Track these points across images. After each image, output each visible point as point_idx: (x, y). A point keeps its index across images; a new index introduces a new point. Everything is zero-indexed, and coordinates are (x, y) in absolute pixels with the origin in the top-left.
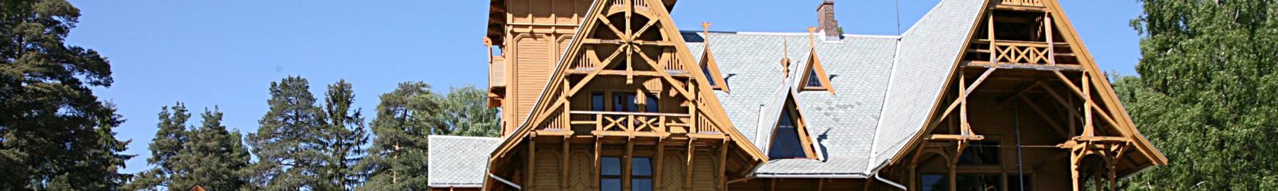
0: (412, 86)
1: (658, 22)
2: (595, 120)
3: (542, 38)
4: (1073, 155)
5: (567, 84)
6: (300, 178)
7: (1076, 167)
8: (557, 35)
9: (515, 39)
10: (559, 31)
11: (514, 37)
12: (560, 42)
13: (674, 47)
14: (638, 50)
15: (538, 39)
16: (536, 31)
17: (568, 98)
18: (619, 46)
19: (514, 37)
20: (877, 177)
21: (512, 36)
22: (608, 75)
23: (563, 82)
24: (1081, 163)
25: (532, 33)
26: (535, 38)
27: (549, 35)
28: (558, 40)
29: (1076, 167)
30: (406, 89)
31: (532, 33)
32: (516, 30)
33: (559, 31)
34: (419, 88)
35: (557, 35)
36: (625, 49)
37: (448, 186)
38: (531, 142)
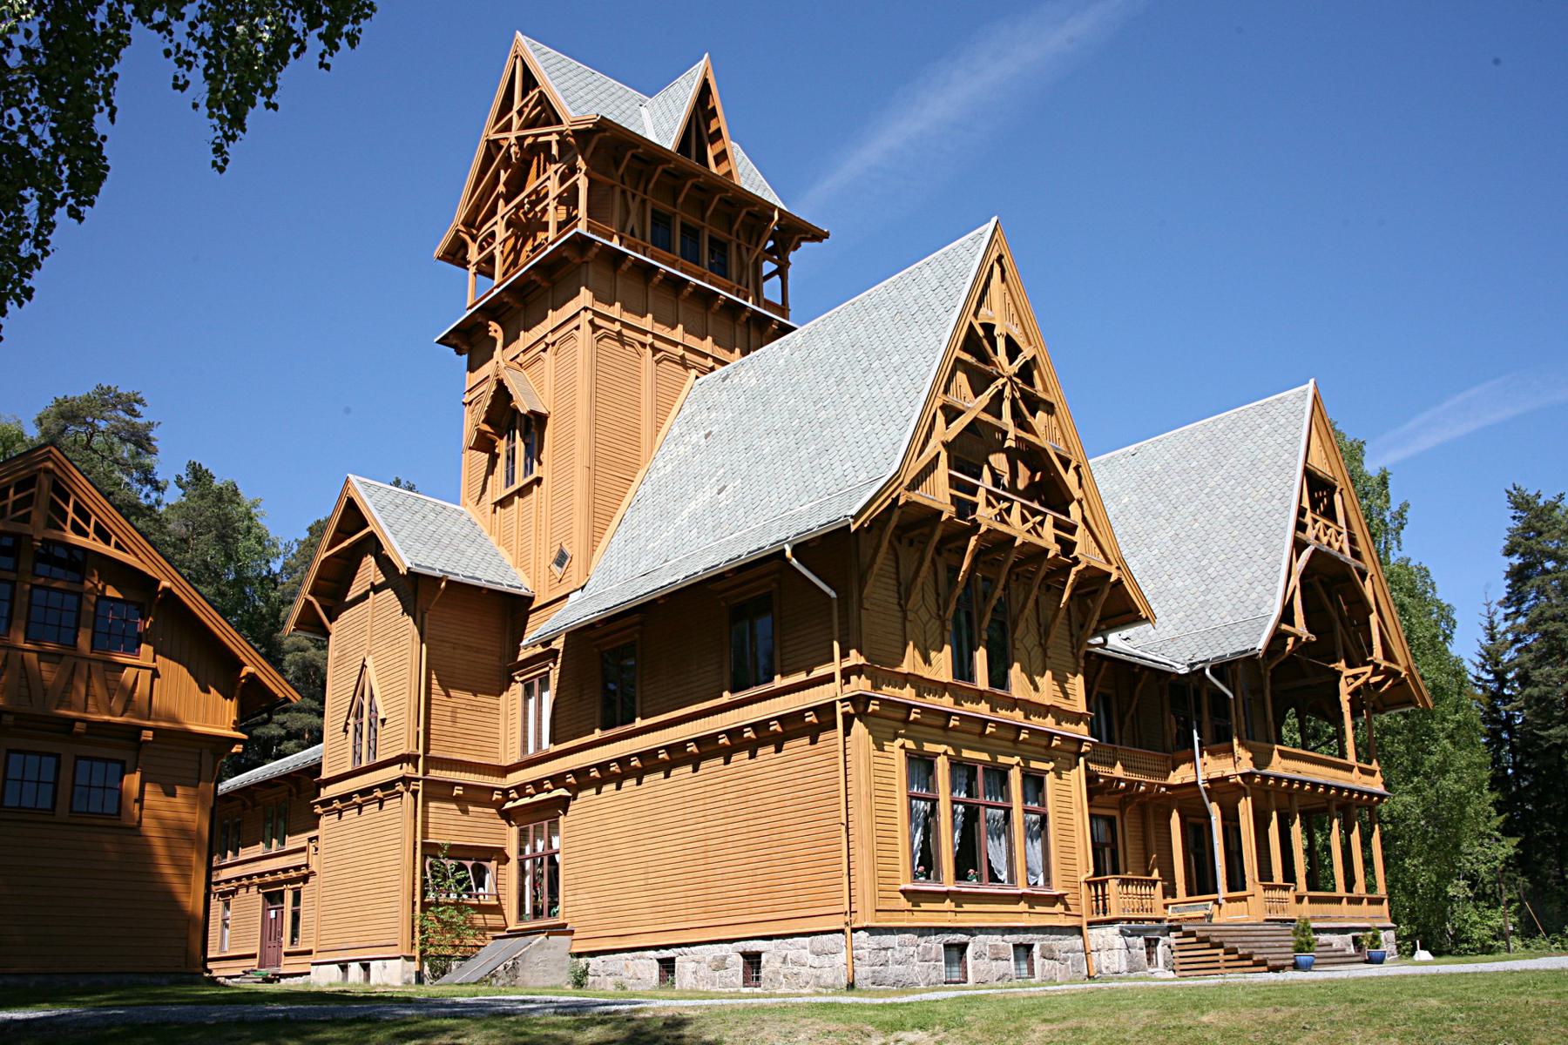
0: (118, 396)
1: (1034, 358)
2: (974, 495)
3: (633, 347)
4: (1343, 679)
5: (940, 419)
6: (202, 497)
7: (1349, 697)
8: (656, 350)
9: (595, 335)
10: (658, 344)
11: (593, 333)
12: (658, 362)
13: (1052, 405)
14: (1018, 395)
15: (627, 347)
16: (625, 332)
17: (946, 445)
18: (996, 379)
19: (593, 333)
20: (1207, 672)
21: (591, 329)
22: (987, 422)
23: (935, 415)
24: (1355, 694)
25: (619, 333)
26: (623, 344)
27: (643, 345)
28: (656, 358)
29: (1349, 697)
30: (109, 399)
31: (619, 333)
32: (598, 321)
33: (658, 344)
34: (129, 404)
35: (656, 350)
36: (1004, 385)
37: (438, 574)
38: (896, 509)
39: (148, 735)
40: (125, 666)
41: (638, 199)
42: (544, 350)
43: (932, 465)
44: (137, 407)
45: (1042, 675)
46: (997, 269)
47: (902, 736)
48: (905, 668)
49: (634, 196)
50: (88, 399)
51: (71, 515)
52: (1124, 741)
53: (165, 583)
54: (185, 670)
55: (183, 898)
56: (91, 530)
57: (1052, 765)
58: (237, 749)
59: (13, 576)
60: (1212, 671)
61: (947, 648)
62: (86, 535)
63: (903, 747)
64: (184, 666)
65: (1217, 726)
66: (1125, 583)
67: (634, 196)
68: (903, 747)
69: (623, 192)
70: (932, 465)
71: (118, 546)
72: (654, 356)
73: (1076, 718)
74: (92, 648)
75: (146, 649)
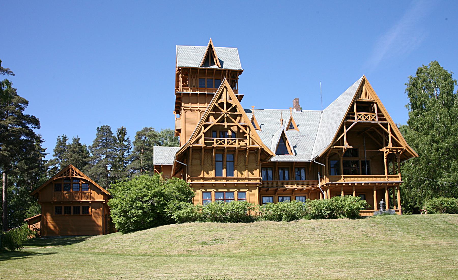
5: (203, 128)
8: (200, 110)
10: (200, 109)
12: (201, 113)
16: (192, 109)
20: (314, 161)
26: (192, 111)
27: (197, 110)
30: (146, 130)
31: (191, 109)
33: (200, 109)
34: (150, 130)
35: (200, 110)
36: (224, 115)
38: (190, 149)
39: (90, 202)
40: (86, 193)
41: (195, 78)
42: (197, 110)
43: (201, 137)
44: (151, 130)
45: (245, 171)
46: (225, 89)
47: (201, 189)
48: (201, 176)
49: (194, 78)
50: (142, 131)
51: (75, 173)
52: (309, 178)
53: (88, 181)
54: (95, 192)
55: (97, 223)
56: (78, 175)
57: (248, 189)
58: (104, 203)
59: (70, 183)
60: (315, 161)
61: (214, 171)
62: (77, 176)
63: (201, 191)
64: (95, 191)
65: (345, 169)
66: (265, 149)
67: (194, 78)
68: (201, 191)
69: (191, 78)
70: (201, 137)
71: (82, 176)
72: (199, 112)
73: (256, 179)
74: (73, 191)
75: (89, 190)
